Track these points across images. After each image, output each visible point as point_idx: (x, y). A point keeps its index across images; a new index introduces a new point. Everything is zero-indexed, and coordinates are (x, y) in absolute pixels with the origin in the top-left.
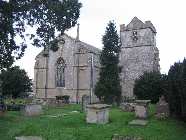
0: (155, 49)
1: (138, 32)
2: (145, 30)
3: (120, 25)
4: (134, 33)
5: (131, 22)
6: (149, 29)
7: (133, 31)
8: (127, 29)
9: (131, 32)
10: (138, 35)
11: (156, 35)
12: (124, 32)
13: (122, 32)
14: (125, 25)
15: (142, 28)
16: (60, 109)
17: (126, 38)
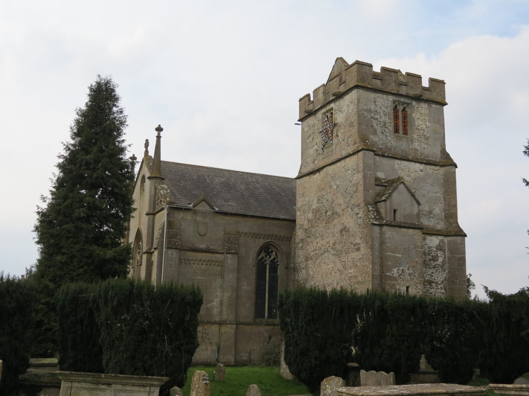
7: (323, 110)
9: (320, 115)
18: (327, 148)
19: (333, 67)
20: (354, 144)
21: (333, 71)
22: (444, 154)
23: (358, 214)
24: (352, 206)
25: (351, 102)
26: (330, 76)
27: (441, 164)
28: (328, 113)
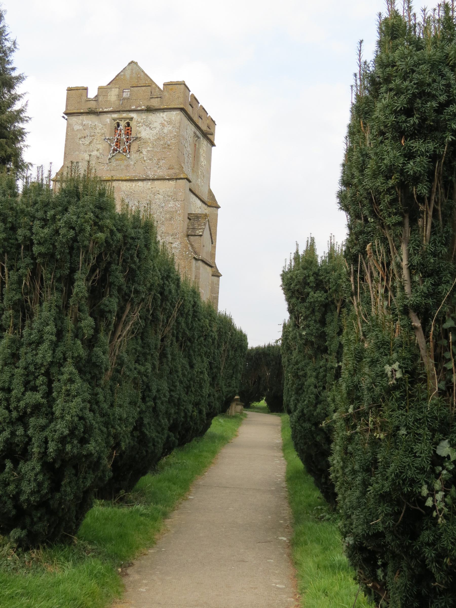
0: (206, 199)
1: (133, 124)
2: (164, 116)
3: (69, 90)
4: (118, 125)
5: (146, 75)
6: (176, 116)
7: (115, 116)
8: (93, 105)
9: (108, 119)
10: (133, 135)
11: (213, 145)
12: (81, 117)
13: (74, 119)
14: (86, 89)
15: (149, 110)
16: (188, 228)
17: (87, 141)
18: (117, 160)
19: (124, 69)
20: (169, 169)
21: (122, 73)
22: (211, 195)
23: (172, 243)
24: (162, 233)
25: (170, 123)
26: (117, 76)
27: (209, 205)
28: (121, 121)
